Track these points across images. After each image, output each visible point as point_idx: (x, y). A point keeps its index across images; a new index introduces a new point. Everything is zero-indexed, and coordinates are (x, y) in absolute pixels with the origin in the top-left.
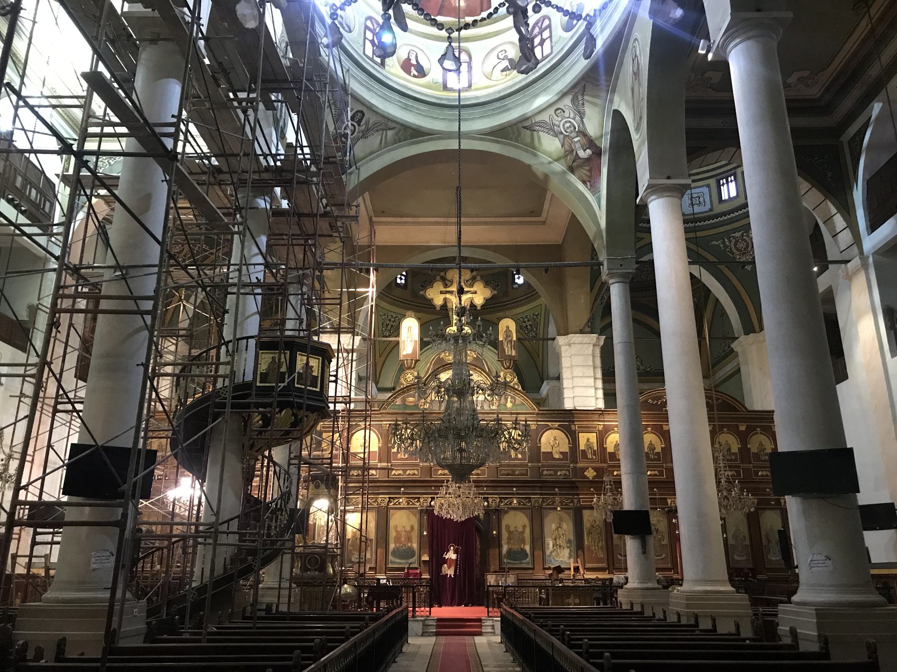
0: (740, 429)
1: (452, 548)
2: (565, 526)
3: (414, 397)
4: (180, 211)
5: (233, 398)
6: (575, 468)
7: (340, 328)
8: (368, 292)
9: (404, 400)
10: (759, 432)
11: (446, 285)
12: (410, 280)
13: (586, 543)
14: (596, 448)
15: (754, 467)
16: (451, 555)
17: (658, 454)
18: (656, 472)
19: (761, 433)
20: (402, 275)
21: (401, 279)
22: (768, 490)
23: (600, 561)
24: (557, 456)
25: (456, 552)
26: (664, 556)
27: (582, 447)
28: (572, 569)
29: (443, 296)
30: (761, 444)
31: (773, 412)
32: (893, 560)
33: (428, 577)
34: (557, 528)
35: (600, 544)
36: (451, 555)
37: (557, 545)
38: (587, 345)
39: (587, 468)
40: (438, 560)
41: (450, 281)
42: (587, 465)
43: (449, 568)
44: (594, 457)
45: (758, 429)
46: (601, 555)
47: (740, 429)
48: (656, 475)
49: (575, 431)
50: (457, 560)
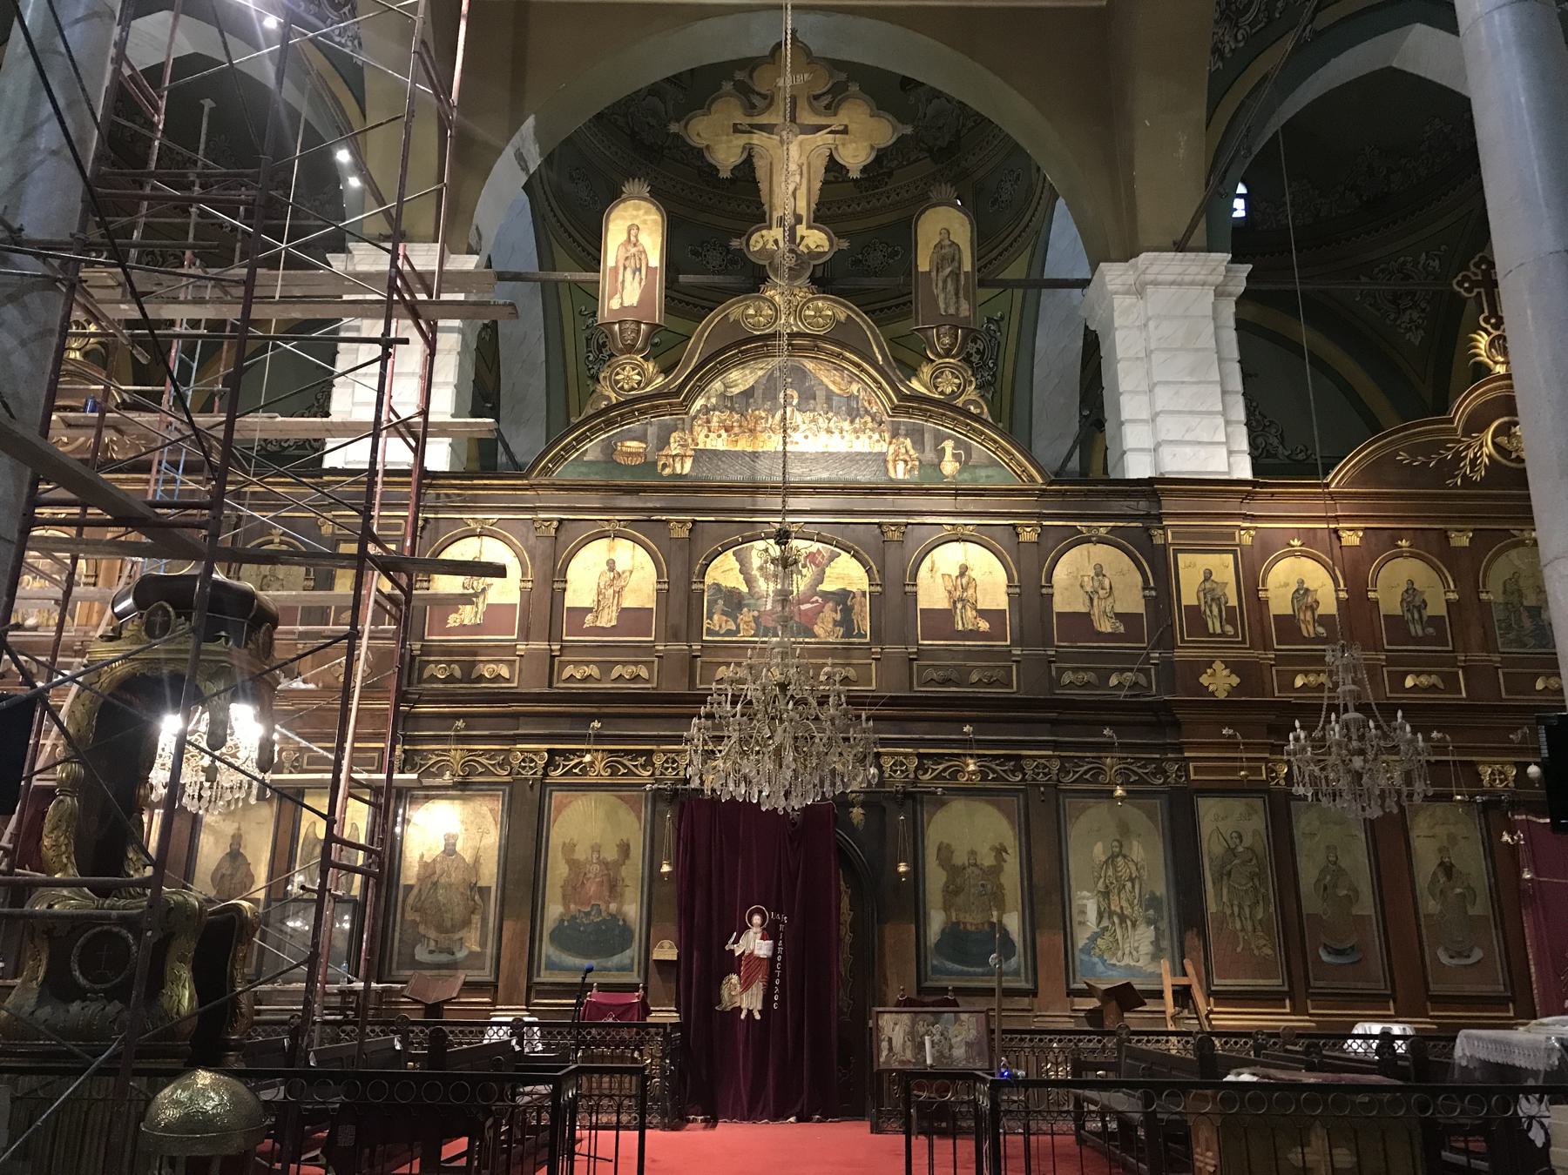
1: (757, 919)
2: (1137, 851)
14: (1233, 602)
15: (1390, 661)
16: (755, 943)
23: (1263, 969)
25: (769, 932)
26: (1477, 954)
27: (1189, 597)
29: (742, 140)
34: (1112, 859)
36: (755, 943)
37: (1111, 914)
39: (1210, 664)
41: (764, 97)
43: (746, 986)
44: (1229, 629)
46: (1266, 948)
50: (772, 960)
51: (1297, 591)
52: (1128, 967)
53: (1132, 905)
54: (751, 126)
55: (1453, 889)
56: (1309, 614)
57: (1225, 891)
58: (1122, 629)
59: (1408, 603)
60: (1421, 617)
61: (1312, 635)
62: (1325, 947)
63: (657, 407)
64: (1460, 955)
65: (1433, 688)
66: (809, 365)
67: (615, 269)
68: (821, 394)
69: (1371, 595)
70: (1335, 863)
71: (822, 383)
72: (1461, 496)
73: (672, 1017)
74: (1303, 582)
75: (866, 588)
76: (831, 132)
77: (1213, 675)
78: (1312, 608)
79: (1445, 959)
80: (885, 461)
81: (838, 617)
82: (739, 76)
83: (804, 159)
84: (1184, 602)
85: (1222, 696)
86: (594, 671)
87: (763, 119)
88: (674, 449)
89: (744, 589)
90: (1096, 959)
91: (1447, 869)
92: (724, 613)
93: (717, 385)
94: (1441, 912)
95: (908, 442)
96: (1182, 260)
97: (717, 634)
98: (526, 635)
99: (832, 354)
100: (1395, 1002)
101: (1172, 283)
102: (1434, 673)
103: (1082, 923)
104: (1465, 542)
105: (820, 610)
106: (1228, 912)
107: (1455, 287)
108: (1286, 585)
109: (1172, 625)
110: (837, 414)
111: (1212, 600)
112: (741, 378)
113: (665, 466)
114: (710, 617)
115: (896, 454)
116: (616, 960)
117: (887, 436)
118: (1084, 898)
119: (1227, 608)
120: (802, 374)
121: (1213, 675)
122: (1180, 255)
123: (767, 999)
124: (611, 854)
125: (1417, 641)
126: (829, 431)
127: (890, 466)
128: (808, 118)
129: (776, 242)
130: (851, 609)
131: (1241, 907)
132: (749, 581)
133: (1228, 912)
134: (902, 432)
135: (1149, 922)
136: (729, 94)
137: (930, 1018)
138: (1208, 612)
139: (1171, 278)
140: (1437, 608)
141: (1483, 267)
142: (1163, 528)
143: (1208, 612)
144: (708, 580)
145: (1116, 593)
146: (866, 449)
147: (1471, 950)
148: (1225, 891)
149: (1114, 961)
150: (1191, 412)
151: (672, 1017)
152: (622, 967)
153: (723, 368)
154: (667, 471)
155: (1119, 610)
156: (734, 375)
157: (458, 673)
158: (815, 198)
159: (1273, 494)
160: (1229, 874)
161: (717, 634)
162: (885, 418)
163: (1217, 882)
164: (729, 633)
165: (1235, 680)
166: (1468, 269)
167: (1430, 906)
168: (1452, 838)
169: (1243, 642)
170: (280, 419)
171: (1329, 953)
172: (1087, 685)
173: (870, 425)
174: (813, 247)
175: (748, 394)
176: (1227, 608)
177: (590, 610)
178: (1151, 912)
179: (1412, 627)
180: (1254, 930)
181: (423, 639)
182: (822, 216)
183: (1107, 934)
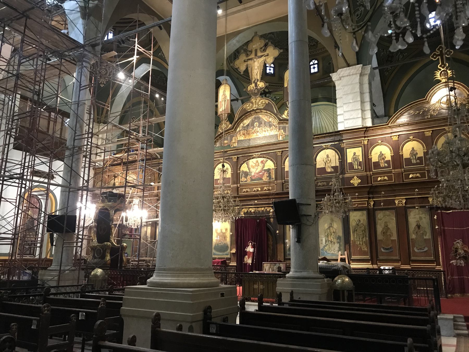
1: (250, 244)
2: (335, 226)
3: (227, 140)
4: (25, 36)
6: (343, 178)
7: (457, 155)
8: (133, 60)
9: (221, 144)
11: (248, 55)
12: (277, 70)
13: (352, 239)
14: (361, 160)
16: (250, 249)
17: (420, 158)
18: (418, 175)
20: (271, 67)
21: (270, 70)
23: (364, 253)
24: (329, 170)
25: (253, 247)
26: (426, 249)
27: (349, 160)
28: (339, 260)
29: (246, 64)
33: (235, 264)
34: (329, 228)
35: (364, 240)
36: (250, 249)
37: (329, 241)
38: (354, 76)
39: (353, 177)
40: (241, 254)
41: (250, 51)
42: (353, 174)
43: (249, 258)
44: (360, 167)
46: (365, 248)
48: (417, 177)
49: (343, 148)
50: (254, 253)
51: (380, 155)
52: (332, 253)
53: (334, 239)
54: (247, 59)
55: (420, 232)
56: (383, 161)
57: (355, 234)
58: (333, 170)
59: (412, 154)
60: (415, 158)
61: (383, 166)
62: (383, 248)
63: (229, 132)
64: (421, 249)
66: (260, 116)
67: (221, 102)
68: (263, 123)
70: (387, 226)
71: (263, 120)
73: (235, 264)
75: (274, 167)
76: (265, 56)
77: (354, 180)
78: (384, 159)
79: (416, 250)
80: (277, 136)
81: (268, 175)
82: (245, 47)
83: (259, 65)
84: (348, 162)
85: (356, 185)
86: (325, 183)
87: (250, 57)
88: (233, 141)
89: (248, 171)
90: (325, 252)
91: (419, 226)
92: (244, 177)
93: (242, 125)
94: (416, 238)
95: (282, 131)
97: (243, 182)
99: (265, 112)
101: (347, 76)
102: (418, 173)
103: (322, 243)
105: (264, 174)
106: (356, 240)
108: (377, 154)
109: (345, 168)
110: (267, 126)
112: (247, 122)
113: (232, 145)
114: (241, 178)
115: (280, 134)
116: (226, 253)
117: (278, 130)
118: (322, 237)
119: (359, 162)
120: (259, 118)
121: (354, 180)
122: (348, 68)
123: (253, 261)
124: (224, 231)
125: (414, 164)
126: (265, 131)
127: (278, 137)
128: (259, 54)
129: (253, 87)
130: (270, 173)
131: (359, 238)
132: (249, 169)
133: (356, 240)
134: (281, 128)
135: (338, 243)
136: (243, 53)
137: (274, 265)
139: (347, 74)
140: (421, 154)
141: (441, 49)
142: (343, 143)
144: (241, 170)
145: (332, 161)
146: (273, 134)
147: (424, 248)
148: (355, 234)
149: (329, 252)
150: (352, 110)
151: (235, 264)
152: (226, 255)
153: (242, 120)
154: (232, 146)
155: (332, 165)
156: (245, 121)
157: (260, 189)
158: (261, 74)
159: (373, 129)
160: (357, 230)
161: (243, 182)
162: (277, 126)
163: (354, 232)
164: (245, 181)
165: (360, 181)
166: (435, 51)
167: (413, 236)
168: (421, 218)
169: (363, 170)
170: (159, 149)
172: (324, 185)
173: (274, 128)
174: (261, 86)
175: (248, 125)
176: (359, 162)
177: (219, 179)
178: (338, 240)
179: (412, 161)
180: (363, 244)
182: (262, 79)
183: (328, 246)
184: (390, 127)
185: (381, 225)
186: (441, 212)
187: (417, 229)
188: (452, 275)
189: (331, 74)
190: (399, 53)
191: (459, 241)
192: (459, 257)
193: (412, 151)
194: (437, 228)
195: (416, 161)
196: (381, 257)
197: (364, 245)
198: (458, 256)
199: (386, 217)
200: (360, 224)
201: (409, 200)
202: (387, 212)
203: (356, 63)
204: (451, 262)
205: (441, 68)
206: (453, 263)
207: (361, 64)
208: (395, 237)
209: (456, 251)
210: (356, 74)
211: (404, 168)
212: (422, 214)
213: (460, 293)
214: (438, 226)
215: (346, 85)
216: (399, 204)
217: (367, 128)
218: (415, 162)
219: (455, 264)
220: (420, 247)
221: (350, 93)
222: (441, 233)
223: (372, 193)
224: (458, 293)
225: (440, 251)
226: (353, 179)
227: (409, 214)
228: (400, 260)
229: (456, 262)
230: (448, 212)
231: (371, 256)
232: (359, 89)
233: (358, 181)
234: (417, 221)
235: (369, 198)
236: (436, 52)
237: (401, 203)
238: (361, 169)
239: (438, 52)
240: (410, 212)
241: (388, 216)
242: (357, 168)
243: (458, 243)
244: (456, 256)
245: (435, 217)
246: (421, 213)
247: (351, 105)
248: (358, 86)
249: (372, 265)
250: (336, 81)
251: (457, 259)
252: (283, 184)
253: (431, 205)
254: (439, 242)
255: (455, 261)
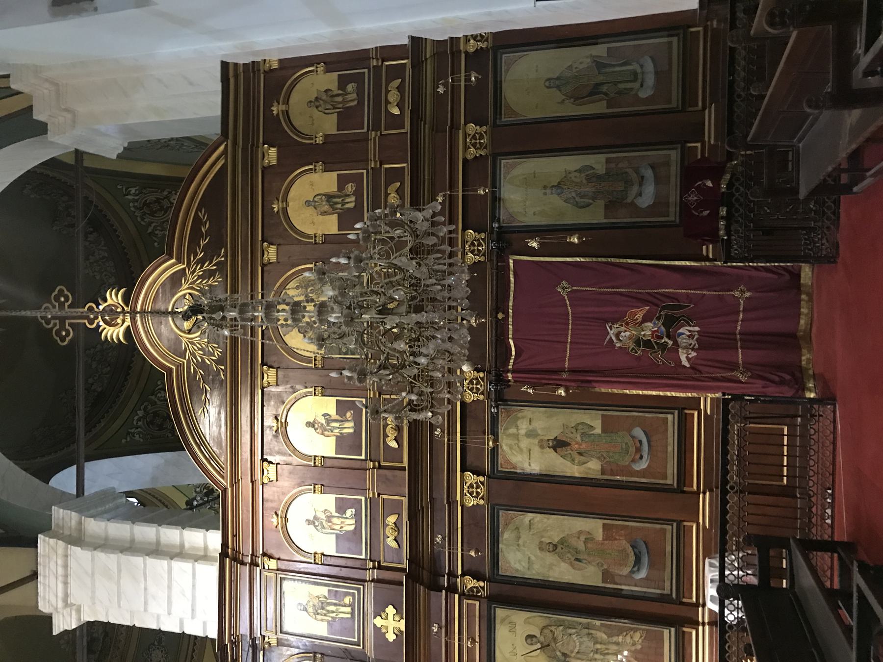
0: (274, 162)
5: (238, 330)
10: (282, 107)
15: (376, 127)
19: (287, 102)
22: (441, 90)
26: (638, 432)
30: (316, 103)
31: (225, 65)
32: (685, 661)
38: (72, 563)
45: (275, 110)
47: (274, 162)
56: (335, 520)
61: (353, 521)
64: (639, 450)
65: (400, 89)
69: (320, 140)
72: (235, 143)
74: (308, 520)
78: (329, 197)
79: (643, 465)
85: (402, 625)
91: (559, 445)
94: (599, 458)
96: (45, 576)
98: (363, 491)
100: (684, 521)
101: (66, 583)
104: (273, 152)
107: (65, 343)
111: (323, 608)
122: (40, 578)
138: (334, 615)
139: (60, 586)
143: (334, 615)
147: (633, 437)
150: (169, 587)
159: (234, 536)
160: (564, 655)
165: (390, 610)
168: (531, 434)
169: (358, 590)
171: (638, 570)
179: (347, 206)
181: (365, 560)
184: (235, 482)
185: (551, 566)
186: (513, 371)
187: (567, 451)
188: (733, 366)
189: (56, 632)
190: (153, 397)
191: (612, 333)
192: (669, 337)
193: (316, 429)
194: (566, 391)
195: (347, 421)
196: (668, 588)
197: (620, 639)
198: (665, 339)
199: (521, 542)
200: (542, 639)
201: (469, 462)
202: (506, 536)
203: (33, 549)
204: (685, 363)
205: (96, 322)
206: (688, 359)
207: (37, 538)
208: (594, 526)
209: (647, 344)
210: (66, 556)
211: (366, 460)
212: (517, 427)
213: (798, 350)
214: (559, 386)
215: (93, 592)
216: (478, 389)
217: (223, 555)
218: (352, 424)
219: (694, 354)
220: (632, 450)
221: (118, 583)
222: (583, 381)
223: (436, 573)
224: (800, 356)
225: (646, 392)
226: (384, 630)
227: (515, 468)
228: (679, 523)
229: (685, 348)
230: (513, 353)
231: (666, 621)
232: (112, 555)
233: (391, 617)
234: (542, 447)
235: (452, 589)
236: (52, 329)
237: (478, 487)
238: (353, 595)
239: (55, 325)
240: (508, 462)
241: (519, 538)
242: (349, 609)
243: (618, 335)
244: (664, 346)
245: (534, 245)
246: (512, 430)
247: (152, 589)
248: (101, 556)
249: (697, 623)
250: (79, 619)
251: (676, 343)
252: (380, 467)
253: (488, 398)
254: (616, 391)
255: (680, 350)
